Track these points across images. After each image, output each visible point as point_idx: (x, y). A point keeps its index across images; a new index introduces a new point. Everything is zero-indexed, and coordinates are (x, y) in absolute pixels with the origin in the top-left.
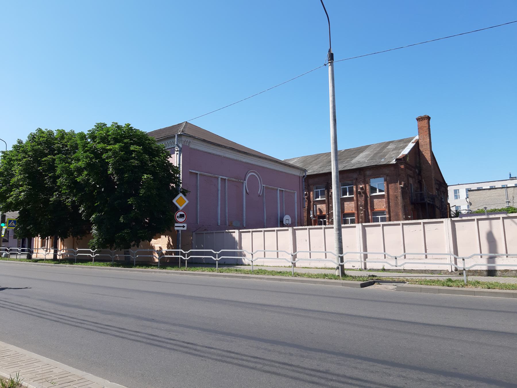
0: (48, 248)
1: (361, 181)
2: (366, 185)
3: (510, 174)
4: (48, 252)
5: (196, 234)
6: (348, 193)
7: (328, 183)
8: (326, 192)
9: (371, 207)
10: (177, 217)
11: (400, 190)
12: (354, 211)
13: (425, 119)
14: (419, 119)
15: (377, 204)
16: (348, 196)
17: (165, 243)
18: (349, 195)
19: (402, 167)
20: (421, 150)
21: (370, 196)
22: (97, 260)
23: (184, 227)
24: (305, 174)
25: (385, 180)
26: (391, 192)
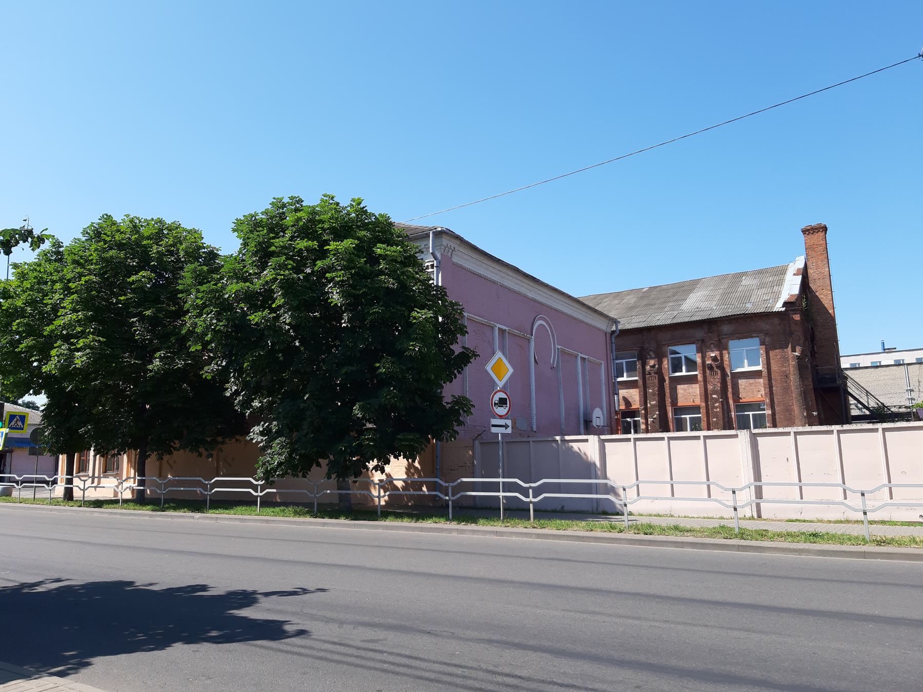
0: (96, 475)
1: (712, 344)
2: (723, 352)
3: (883, 343)
4: (95, 484)
5: (481, 443)
6: (684, 368)
7: (642, 347)
8: (639, 365)
9: (733, 394)
10: (495, 404)
11: (792, 362)
12: (698, 401)
13: (819, 231)
14: (808, 230)
15: (744, 389)
16: (684, 373)
17: (401, 465)
18: (688, 371)
19: (797, 317)
20: (812, 288)
21: (731, 373)
22: (268, 502)
23: (506, 426)
24: (617, 327)
25: (762, 343)
26: (774, 367)
